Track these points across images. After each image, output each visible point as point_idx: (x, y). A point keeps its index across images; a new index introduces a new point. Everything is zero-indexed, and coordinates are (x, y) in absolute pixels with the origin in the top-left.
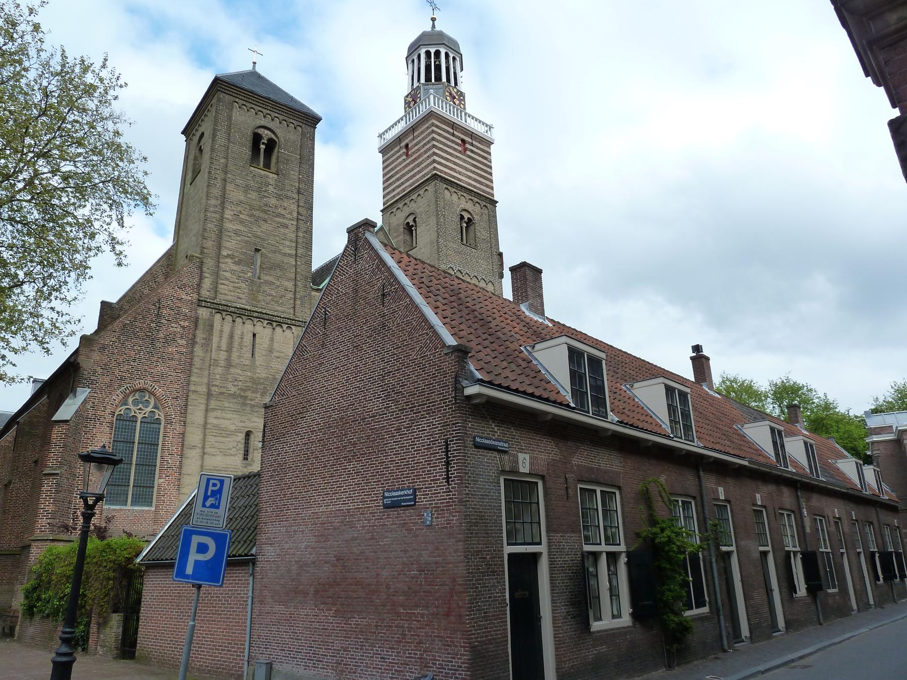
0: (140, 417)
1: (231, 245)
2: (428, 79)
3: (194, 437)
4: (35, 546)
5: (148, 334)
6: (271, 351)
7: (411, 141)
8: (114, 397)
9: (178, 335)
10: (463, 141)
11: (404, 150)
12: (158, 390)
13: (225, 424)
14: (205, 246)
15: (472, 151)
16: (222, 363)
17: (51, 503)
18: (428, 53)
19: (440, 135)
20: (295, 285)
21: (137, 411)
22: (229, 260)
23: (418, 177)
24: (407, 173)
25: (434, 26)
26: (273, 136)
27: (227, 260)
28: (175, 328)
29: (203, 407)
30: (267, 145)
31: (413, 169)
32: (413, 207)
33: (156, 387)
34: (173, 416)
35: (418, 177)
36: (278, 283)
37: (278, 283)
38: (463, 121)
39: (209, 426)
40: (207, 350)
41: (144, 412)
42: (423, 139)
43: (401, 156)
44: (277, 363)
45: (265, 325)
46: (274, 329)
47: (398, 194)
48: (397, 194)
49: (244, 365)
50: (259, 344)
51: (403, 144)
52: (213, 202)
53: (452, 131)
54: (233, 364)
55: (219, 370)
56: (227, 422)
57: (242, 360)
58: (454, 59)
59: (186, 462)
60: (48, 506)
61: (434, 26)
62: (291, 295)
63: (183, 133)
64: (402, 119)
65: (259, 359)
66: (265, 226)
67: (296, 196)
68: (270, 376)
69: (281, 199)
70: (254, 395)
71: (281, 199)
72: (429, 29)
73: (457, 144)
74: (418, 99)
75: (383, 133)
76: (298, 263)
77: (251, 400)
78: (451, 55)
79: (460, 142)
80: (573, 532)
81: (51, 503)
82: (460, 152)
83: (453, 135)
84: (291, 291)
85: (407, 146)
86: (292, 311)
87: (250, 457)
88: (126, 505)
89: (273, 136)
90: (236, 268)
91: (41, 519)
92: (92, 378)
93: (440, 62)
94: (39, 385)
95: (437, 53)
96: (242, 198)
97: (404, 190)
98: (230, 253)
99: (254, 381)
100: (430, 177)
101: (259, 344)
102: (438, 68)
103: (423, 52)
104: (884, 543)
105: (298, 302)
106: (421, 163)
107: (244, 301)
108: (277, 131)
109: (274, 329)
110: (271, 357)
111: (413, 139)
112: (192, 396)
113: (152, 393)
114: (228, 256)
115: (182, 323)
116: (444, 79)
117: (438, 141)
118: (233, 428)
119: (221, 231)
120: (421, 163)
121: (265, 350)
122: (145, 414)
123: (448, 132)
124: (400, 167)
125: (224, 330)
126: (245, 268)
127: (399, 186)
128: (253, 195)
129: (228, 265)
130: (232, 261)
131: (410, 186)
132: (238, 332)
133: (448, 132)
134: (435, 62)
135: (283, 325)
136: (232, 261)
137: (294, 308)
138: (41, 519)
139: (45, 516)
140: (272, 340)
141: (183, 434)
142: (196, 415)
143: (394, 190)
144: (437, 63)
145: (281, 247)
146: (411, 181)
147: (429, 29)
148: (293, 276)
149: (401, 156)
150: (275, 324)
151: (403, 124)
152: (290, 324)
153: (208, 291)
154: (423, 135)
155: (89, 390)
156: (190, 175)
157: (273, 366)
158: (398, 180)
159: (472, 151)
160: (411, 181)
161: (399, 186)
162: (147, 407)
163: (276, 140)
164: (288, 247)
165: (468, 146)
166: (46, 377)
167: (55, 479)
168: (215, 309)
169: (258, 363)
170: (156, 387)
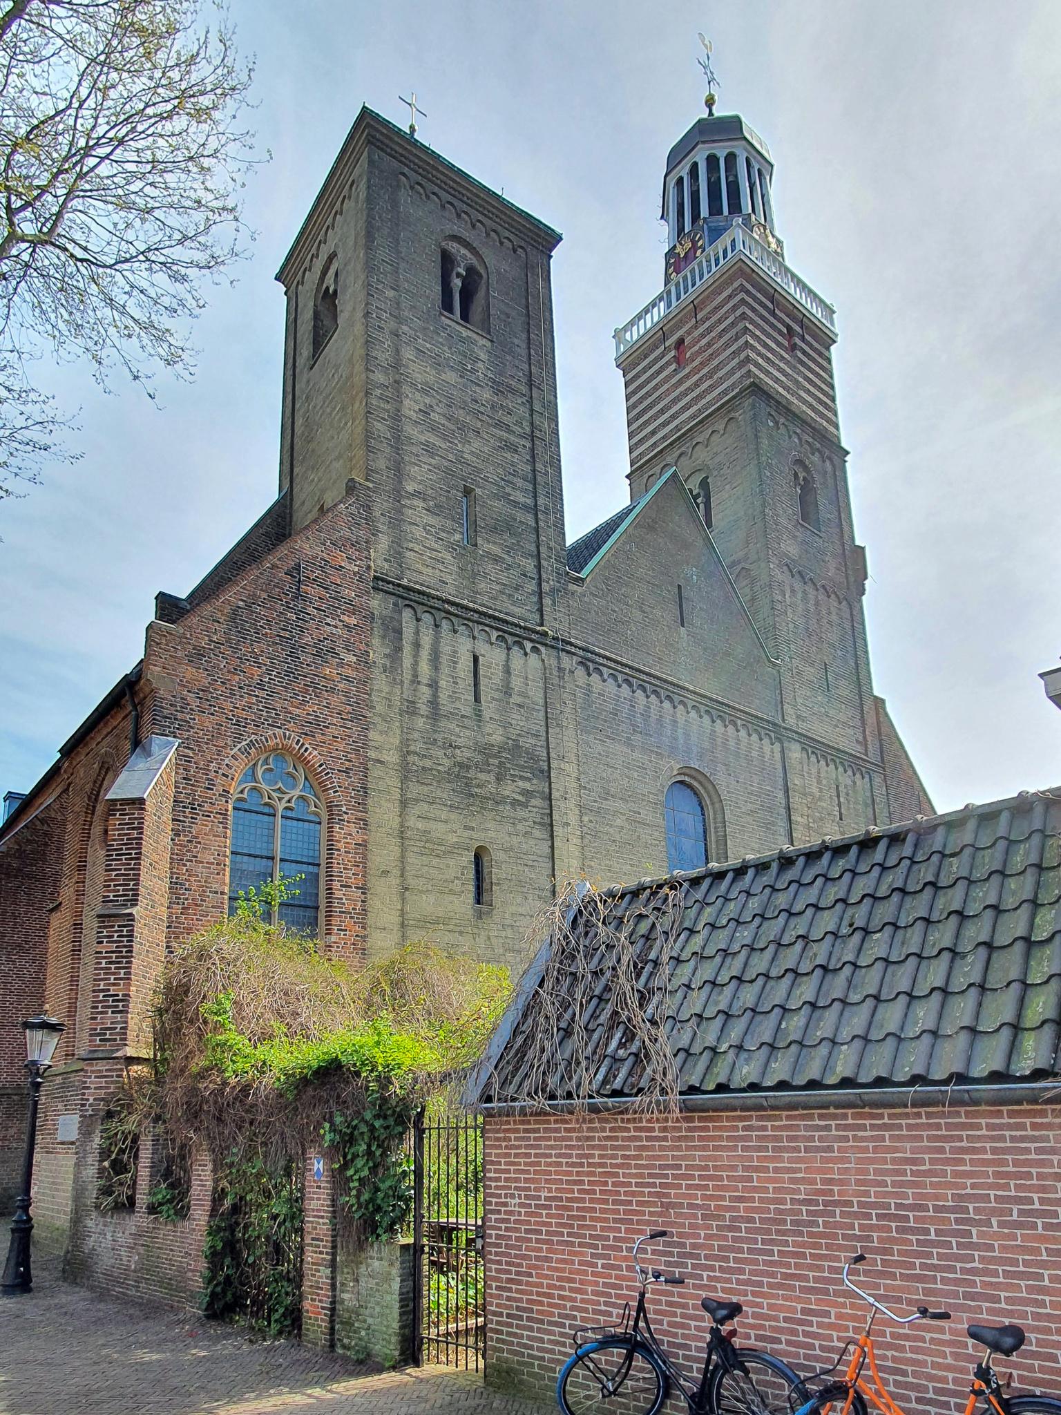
0: (281, 807)
1: (419, 475)
3: (384, 854)
4: (92, 1072)
5: (283, 633)
6: (507, 690)
7: (689, 333)
8: (227, 761)
9: (340, 643)
10: (789, 328)
12: (310, 753)
13: (438, 829)
14: (373, 465)
15: (804, 353)
16: (424, 709)
17: (121, 979)
19: (753, 310)
20: (539, 567)
21: (274, 795)
22: (419, 503)
23: (709, 398)
24: (684, 394)
25: (711, 113)
26: (475, 261)
27: (416, 503)
28: (334, 628)
29: (397, 794)
30: (465, 280)
31: (697, 385)
32: (701, 455)
33: (307, 746)
34: (344, 809)
35: (709, 398)
36: (509, 560)
37: (509, 560)
39: (409, 834)
40: (394, 679)
41: (287, 797)
42: (720, 321)
43: (668, 364)
44: (519, 717)
45: (493, 639)
46: (509, 649)
47: (664, 438)
48: (663, 438)
49: (463, 716)
50: (485, 676)
51: (671, 341)
52: (379, 377)
54: (441, 712)
55: (420, 723)
56: (441, 827)
57: (459, 706)
59: (374, 903)
60: (114, 984)
61: (711, 113)
62: (531, 587)
63: (277, 278)
64: (660, 298)
65: (489, 710)
66: (476, 444)
67: (524, 390)
68: (510, 742)
69: (501, 391)
70: (483, 777)
71: (501, 391)
72: (705, 116)
73: (780, 332)
74: (699, 251)
75: (625, 329)
76: (541, 524)
77: (478, 786)
79: (785, 331)
81: (121, 979)
82: (786, 350)
83: (773, 314)
84: (534, 579)
86: (537, 617)
87: (485, 897)
89: (475, 261)
90: (432, 520)
91: (102, 1013)
92: (180, 716)
93: (736, 176)
94: (16, 804)
96: (431, 379)
97: (677, 428)
98: (420, 488)
99: (485, 750)
100: (741, 392)
101: (485, 676)
105: (547, 601)
106: (718, 368)
107: (451, 589)
108: (483, 251)
109: (509, 649)
110: (508, 703)
111: (696, 327)
112: (376, 772)
113: (301, 760)
114: (416, 494)
115: (345, 618)
117: (752, 322)
118: (452, 839)
119: (398, 440)
120: (718, 368)
121: (497, 690)
122: (289, 801)
123: (765, 307)
124: (666, 387)
125: (422, 642)
126: (449, 523)
127: (664, 424)
128: (451, 376)
129: (417, 512)
130: (425, 506)
131: (693, 417)
132: (446, 649)
133: (765, 307)
135: (525, 642)
136: (425, 506)
137: (541, 611)
138: (102, 1013)
139: (109, 1007)
140: (507, 670)
141: (363, 845)
142: (384, 811)
143: (653, 433)
144: (731, 179)
145: (508, 490)
146: (695, 408)
147: (705, 116)
148: (533, 548)
149: (668, 364)
150: (510, 639)
151: (657, 314)
152: (538, 643)
153: (385, 560)
154: (717, 316)
155: (177, 742)
156: (305, 351)
157: (513, 722)
158: (662, 411)
159: (804, 353)
160: (695, 408)
161: (664, 424)
162: (294, 787)
163: (482, 271)
164: (521, 490)
165: (797, 340)
166: (27, 791)
167: (125, 926)
168: (403, 597)
169: (487, 714)
170: (307, 746)
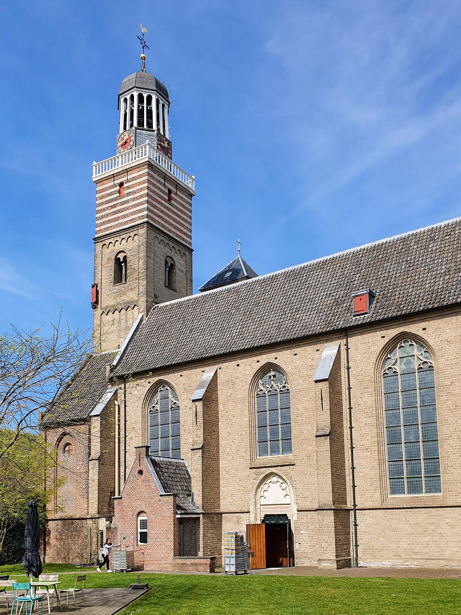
2: (140, 123)
11: (118, 188)
18: (141, 96)
38: (172, 173)
51: (118, 181)
53: (163, 181)
58: (163, 105)
78: (161, 102)
80: (222, 558)
82: (165, 200)
85: (121, 184)
88: (351, 559)
95: (149, 98)
102: (150, 112)
103: (136, 94)
104: (144, 209)
116: (155, 127)
123: (159, 182)
133: (159, 182)
134: (147, 108)
